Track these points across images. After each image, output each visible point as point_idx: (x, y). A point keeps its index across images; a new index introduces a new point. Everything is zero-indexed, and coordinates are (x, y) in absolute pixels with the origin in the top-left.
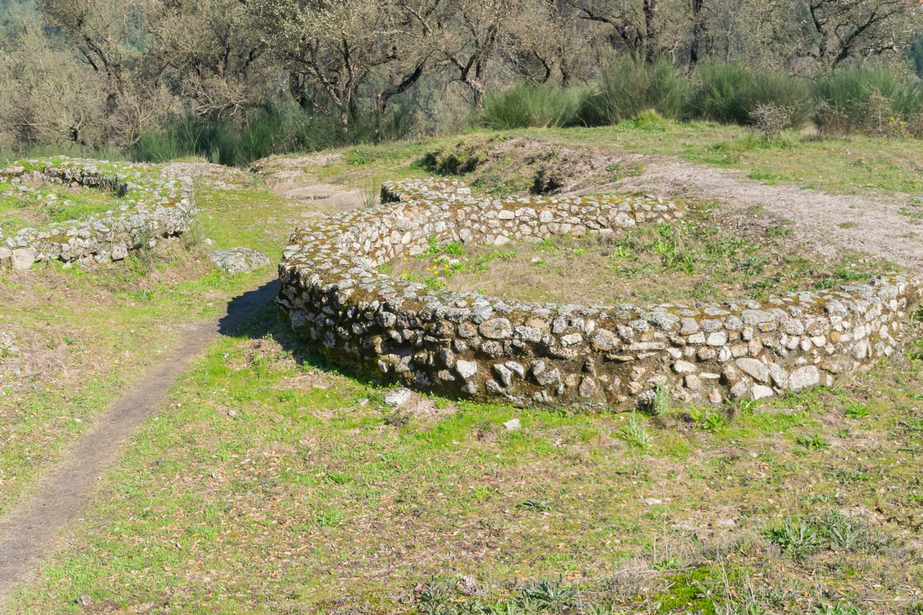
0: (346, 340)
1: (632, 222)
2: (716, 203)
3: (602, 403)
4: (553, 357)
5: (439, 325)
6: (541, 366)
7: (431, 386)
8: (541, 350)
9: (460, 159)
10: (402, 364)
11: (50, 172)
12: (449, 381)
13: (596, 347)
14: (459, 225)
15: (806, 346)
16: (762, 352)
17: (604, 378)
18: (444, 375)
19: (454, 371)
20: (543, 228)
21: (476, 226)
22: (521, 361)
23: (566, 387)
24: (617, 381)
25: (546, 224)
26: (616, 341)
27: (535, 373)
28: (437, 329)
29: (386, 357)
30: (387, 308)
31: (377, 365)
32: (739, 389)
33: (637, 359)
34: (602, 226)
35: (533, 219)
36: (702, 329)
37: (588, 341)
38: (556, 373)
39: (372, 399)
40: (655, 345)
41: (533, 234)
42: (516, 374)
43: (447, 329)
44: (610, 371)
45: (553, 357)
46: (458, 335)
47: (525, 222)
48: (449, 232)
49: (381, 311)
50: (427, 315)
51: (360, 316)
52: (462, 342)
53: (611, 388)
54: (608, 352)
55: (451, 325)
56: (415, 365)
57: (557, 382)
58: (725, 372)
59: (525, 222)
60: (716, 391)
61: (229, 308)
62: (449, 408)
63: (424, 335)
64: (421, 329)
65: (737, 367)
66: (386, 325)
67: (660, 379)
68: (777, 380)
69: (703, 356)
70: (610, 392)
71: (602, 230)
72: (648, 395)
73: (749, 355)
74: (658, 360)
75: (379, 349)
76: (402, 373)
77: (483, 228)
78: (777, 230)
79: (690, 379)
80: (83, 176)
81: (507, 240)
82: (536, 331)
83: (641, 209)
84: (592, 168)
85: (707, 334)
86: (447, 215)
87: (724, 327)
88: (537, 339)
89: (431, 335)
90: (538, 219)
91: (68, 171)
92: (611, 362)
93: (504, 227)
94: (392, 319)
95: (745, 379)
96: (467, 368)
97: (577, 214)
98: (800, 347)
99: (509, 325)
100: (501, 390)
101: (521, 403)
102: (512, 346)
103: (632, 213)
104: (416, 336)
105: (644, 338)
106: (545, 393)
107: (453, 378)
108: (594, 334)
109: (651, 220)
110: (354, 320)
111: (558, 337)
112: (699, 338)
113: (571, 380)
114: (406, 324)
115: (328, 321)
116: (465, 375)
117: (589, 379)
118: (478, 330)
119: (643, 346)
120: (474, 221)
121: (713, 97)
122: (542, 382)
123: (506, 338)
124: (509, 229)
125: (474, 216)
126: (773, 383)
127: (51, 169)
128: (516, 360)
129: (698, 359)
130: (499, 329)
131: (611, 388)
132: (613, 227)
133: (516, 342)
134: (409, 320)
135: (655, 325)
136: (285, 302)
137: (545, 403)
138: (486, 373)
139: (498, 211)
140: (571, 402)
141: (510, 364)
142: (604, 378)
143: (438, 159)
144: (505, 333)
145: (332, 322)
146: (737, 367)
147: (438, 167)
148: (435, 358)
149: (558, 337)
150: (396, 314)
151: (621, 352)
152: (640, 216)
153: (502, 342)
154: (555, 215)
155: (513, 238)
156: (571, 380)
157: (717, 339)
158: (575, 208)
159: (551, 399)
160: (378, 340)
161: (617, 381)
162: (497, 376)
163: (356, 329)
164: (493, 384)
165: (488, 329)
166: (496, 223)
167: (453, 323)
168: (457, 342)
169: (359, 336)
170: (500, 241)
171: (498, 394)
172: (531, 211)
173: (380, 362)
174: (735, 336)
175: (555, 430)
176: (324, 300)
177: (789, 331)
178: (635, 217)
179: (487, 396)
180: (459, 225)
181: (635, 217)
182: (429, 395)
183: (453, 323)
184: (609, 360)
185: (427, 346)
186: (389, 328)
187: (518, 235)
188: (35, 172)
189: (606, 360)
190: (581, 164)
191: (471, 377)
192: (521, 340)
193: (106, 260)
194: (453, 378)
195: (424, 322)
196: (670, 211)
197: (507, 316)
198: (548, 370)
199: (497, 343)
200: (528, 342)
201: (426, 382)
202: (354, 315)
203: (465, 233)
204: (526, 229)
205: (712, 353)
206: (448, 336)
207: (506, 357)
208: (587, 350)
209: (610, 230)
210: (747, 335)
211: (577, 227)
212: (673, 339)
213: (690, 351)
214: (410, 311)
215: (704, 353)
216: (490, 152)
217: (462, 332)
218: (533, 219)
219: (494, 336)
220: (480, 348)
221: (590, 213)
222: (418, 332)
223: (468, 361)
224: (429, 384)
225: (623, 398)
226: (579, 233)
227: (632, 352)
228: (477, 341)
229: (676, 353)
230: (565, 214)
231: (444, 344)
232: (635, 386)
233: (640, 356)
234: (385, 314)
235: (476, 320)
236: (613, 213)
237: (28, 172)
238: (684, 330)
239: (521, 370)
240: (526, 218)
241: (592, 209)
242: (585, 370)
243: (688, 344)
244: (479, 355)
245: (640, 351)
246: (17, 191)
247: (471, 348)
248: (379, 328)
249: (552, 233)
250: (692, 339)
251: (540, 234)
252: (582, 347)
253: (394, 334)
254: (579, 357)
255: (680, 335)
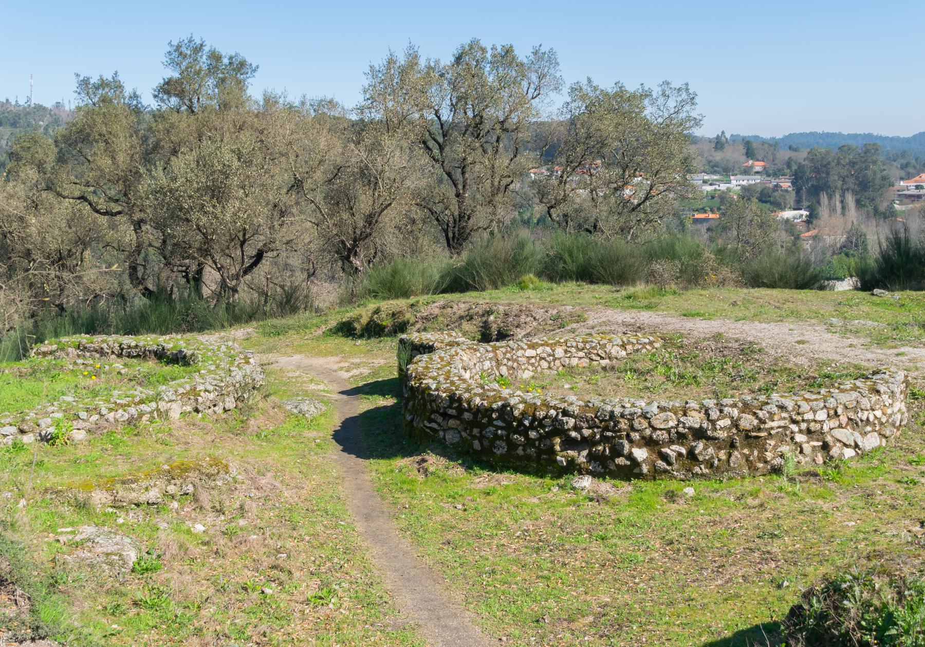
0: (519, 445)
1: (624, 353)
2: (682, 336)
3: (745, 471)
4: (708, 438)
5: (617, 423)
6: (700, 446)
7: (605, 472)
8: (700, 434)
9: (384, 323)
10: (581, 457)
11: (85, 348)
12: (625, 465)
13: (741, 427)
14: (499, 364)
15: (871, 418)
16: (847, 424)
17: (746, 451)
18: (621, 461)
19: (630, 457)
20: (557, 362)
21: (510, 363)
22: (682, 444)
23: (719, 460)
24: (756, 453)
25: (559, 359)
26: (756, 422)
27: (696, 452)
28: (615, 425)
29: (564, 453)
30: (565, 413)
31: (556, 461)
32: (835, 451)
33: (770, 434)
34: (602, 358)
35: (549, 355)
36: (811, 409)
37: (735, 424)
38: (711, 450)
39: (561, 487)
40: (782, 423)
41: (549, 368)
42: (680, 454)
43: (624, 424)
44: (750, 446)
45: (708, 438)
46: (632, 428)
47: (544, 359)
48: (492, 370)
49: (560, 417)
50: (605, 416)
51: (538, 424)
52: (637, 434)
53: (751, 458)
54: (749, 431)
55: (626, 421)
56: (591, 457)
57: (712, 457)
58: (827, 440)
59: (544, 359)
60: (819, 455)
61: (336, 441)
62: (626, 487)
63: (603, 431)
64: (598, 427)
65: (832, 436)
66: (566, 427)
67: (785, 448)
68: (860, 444)
69: (813, 429)
70: (751, 462)
71: (602, 361)
72: (778, 461)
73: (840, 426)
74: (785, 436)
75: (558, 448)
76: (579, 465)
77: (515, 365)
78: (747, 350)
79: (805, 446)
80: (122, 349)
81: (532, 374)
82: (695, 420)
83: (629, 343)
84: (535, 318)
85: (815, 412)
86: (491, 355)
87: (825, 406)
88: (697, 426)
89: (609, 431)
90: (553, 355)
91: (105, 346)
92: (751, 438)
93: (529, 364)
94: (572, 422)
95: (838, 444)
96: (641, 454)
97: (583, 349)
98: (868, 419)
99: (674, 417)
100: (668, 468)
101: (682, 477)
102: (677, 432)
103: (623, 346)
104: (594, 434)
105: (776, 418)
106: (702, 466)
107: (628, 463)
108: (739, 419)
109: (637, 350)
110: (532, 427)
111: (713, 422)
112: (809, 416)
113: (723, 455)
114: (585, 425)
115: (499, 432)
116: (640, 459)
117: (736, 453)
118: (649, 423)
119: (775, 424)
120: (508, 359)
121: (565, 262)
122: (701, 458)
123: (672, 427)
124: (533, 365)
125: (508, 355)
126: (856, 446)
127: (88, 345)
128: (678, 444)
129: (809, 432)
130: (666, 421)
131: (751, 458)
132: (610, 358)
133: (681, 429)
134: (588, 421)
135: (782, 408)
136: (434, 425)
137: (702, 475)
138: (654, 456)
139: (525, 350)
140: (723, 472)
141: (674, 447)
142: (746, 451)
143: (356, 325)
144: (672, 424)
145: (504, 432)
146: (832, 436)
147: (358, 332)
148: (610, 449)
149: (713, 422)
150: (575, 418)
151: (759, 430)
152: (629, 347)
153: (668, 431)
154: (566, 352)
155: (535, 371)
156: (723, 455)
157: (822, 415)
158: (581, 345)
159: (707, 471)
160: (558, 440)
161: (756, 453)
162: (665, 458)
163: (533, 434)
164: (661, 464)
165: (658, 422)
166: (524, 360)
167: (628, 419)
168: (632, 434)
169: (534, 440)
170: (527, 375)
171: (666, 471)
172: (548, 349)
173: (558, 458)
174: (832, 412)
175: (726, 492)
176: (494, 416)
177: (863, 407)
178: (626, 349)
179: (656, 474)
180: (499, 364)
181: (626, 349)
182: (604, 479)
183: (628, 419)
184: (750, 437)
185: (604, 439)
186: (569, 430)
187: (539, 369)
188: (70, 350)
189: (748, 437)
190: (523, 317)
191: (644, 460)
192: (684, 428)
193: (221, 411)
194: (628, 463)
195: (601, 422)
196: (651, 343)
197: (670, 411)
198: (705, 449)
199: (664, 432)
200: (690, 428)
201: (600, 469)
202: (532, 423)
203: (504, 370)
204: (545, 364)
205: (818, 426)
206: (624, 430)
207: (671, 442)
208: (734, 431)
209: (607, 361)
210: (840, 411)
211: (582, 360)
212: (794, 417)
213: (804, 426)
214: (589, 415)
215: (813, 426)
216: (418, 315)
217: (636, 425)
218: (549, 355)
219: (662, 427)
220: (651, 437)
221: (593, 348)
222: (596, 430)
223: (640, 448)
224: (602, 471)
225: (761, 465)
226: (585, 365)
227: (766, 430)
228: (648, 432)
229: (794, 428)
230: (573, 350)
231: (620, 437)
232: (769, 455)
233: (773, 432)
234: (565, 419)
235: (648, 416)
236: (609, 347)
237: (62, 349)
238: (801, 410)
239: (684, 451)
240: (545, 355)
241: (594, 345)
242: (732, 446)
243: (803, 421)
244: (649, 442)
245: (772, 428)
246: (75, 363)
247: (643, 438)
248: (558, 430)
249: (564, 366)
250: (806, 417)
251: (555, 368)
252: (730, 429)
253: (573, 434)
254: (729, 437)
255: (799, 414)
